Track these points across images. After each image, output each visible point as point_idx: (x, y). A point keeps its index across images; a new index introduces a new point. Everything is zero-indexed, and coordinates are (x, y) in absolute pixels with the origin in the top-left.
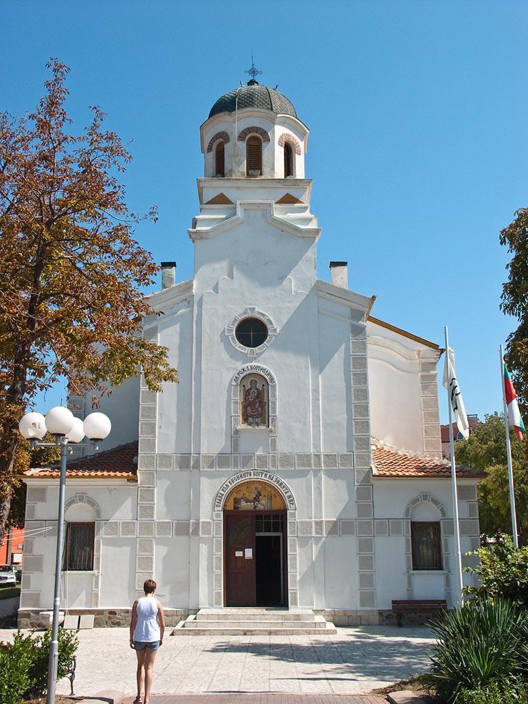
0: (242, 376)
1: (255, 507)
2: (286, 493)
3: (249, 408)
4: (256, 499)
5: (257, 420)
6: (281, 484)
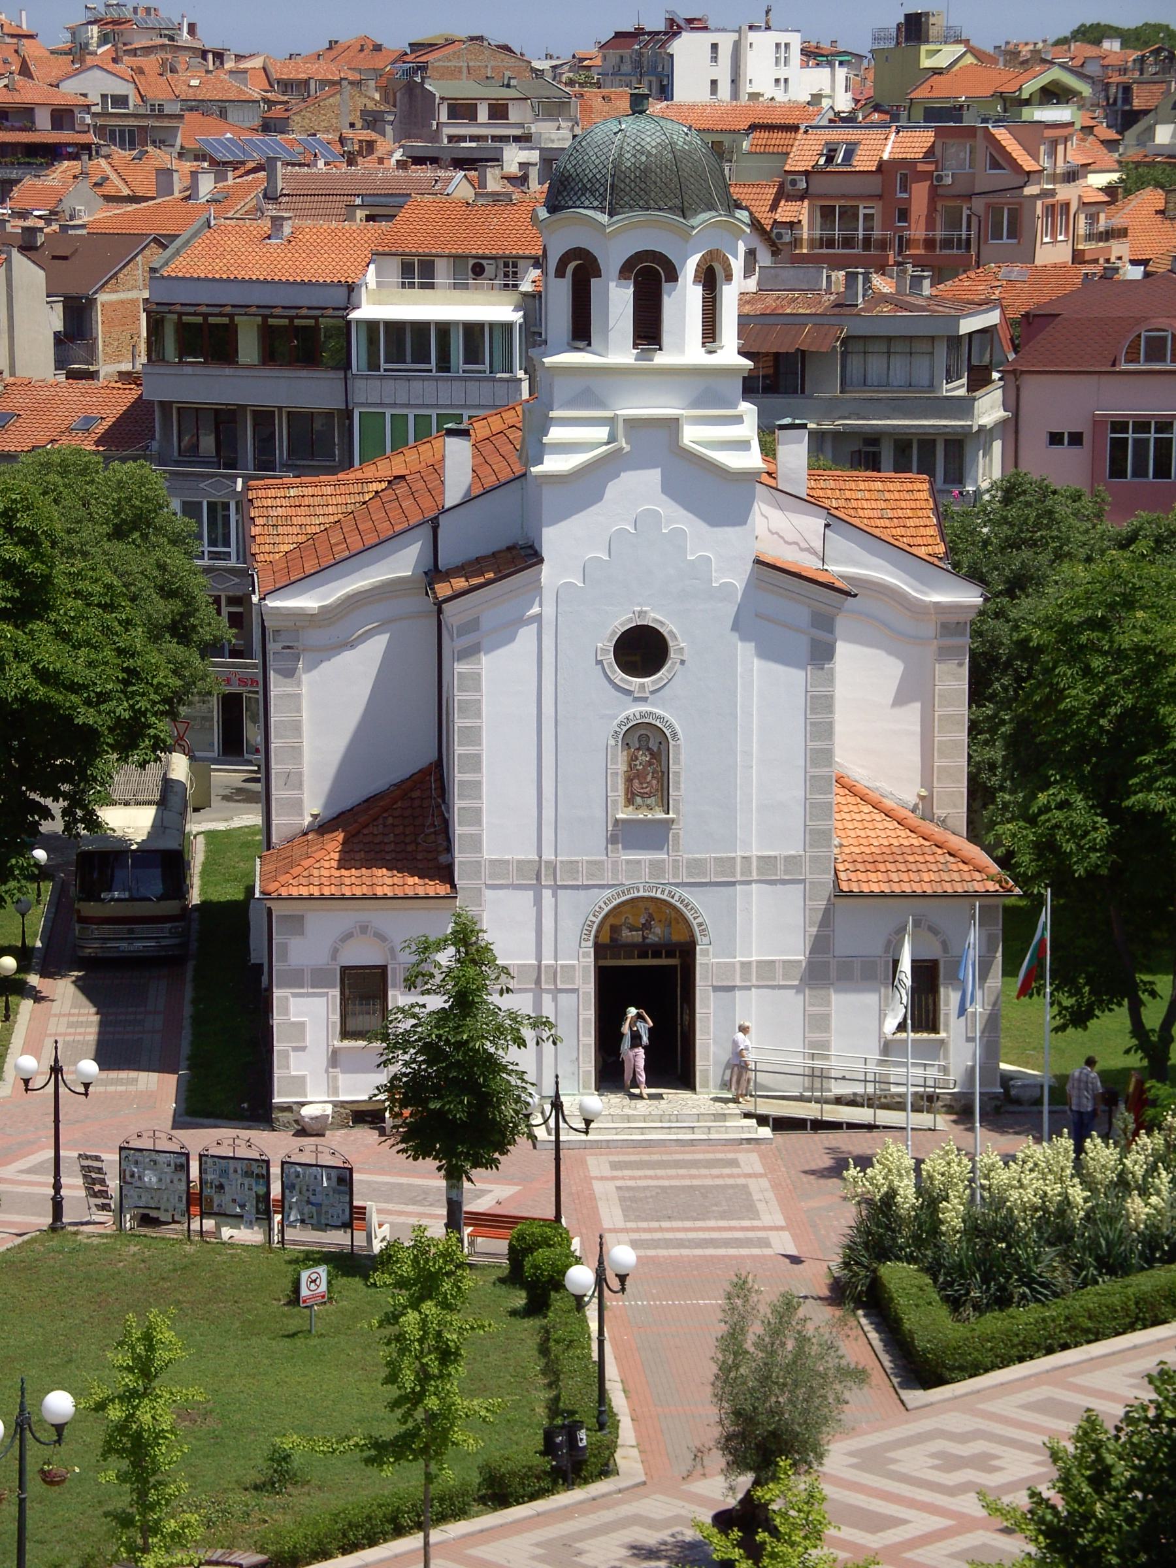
0: (625, 728)
1: (644, 938)
2: (695, 918)
3: (636, 782)
4: (646, 926)
5: (649, 801)
6: (687, 905)
